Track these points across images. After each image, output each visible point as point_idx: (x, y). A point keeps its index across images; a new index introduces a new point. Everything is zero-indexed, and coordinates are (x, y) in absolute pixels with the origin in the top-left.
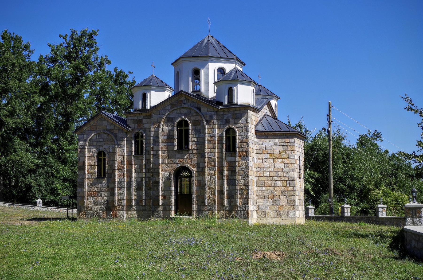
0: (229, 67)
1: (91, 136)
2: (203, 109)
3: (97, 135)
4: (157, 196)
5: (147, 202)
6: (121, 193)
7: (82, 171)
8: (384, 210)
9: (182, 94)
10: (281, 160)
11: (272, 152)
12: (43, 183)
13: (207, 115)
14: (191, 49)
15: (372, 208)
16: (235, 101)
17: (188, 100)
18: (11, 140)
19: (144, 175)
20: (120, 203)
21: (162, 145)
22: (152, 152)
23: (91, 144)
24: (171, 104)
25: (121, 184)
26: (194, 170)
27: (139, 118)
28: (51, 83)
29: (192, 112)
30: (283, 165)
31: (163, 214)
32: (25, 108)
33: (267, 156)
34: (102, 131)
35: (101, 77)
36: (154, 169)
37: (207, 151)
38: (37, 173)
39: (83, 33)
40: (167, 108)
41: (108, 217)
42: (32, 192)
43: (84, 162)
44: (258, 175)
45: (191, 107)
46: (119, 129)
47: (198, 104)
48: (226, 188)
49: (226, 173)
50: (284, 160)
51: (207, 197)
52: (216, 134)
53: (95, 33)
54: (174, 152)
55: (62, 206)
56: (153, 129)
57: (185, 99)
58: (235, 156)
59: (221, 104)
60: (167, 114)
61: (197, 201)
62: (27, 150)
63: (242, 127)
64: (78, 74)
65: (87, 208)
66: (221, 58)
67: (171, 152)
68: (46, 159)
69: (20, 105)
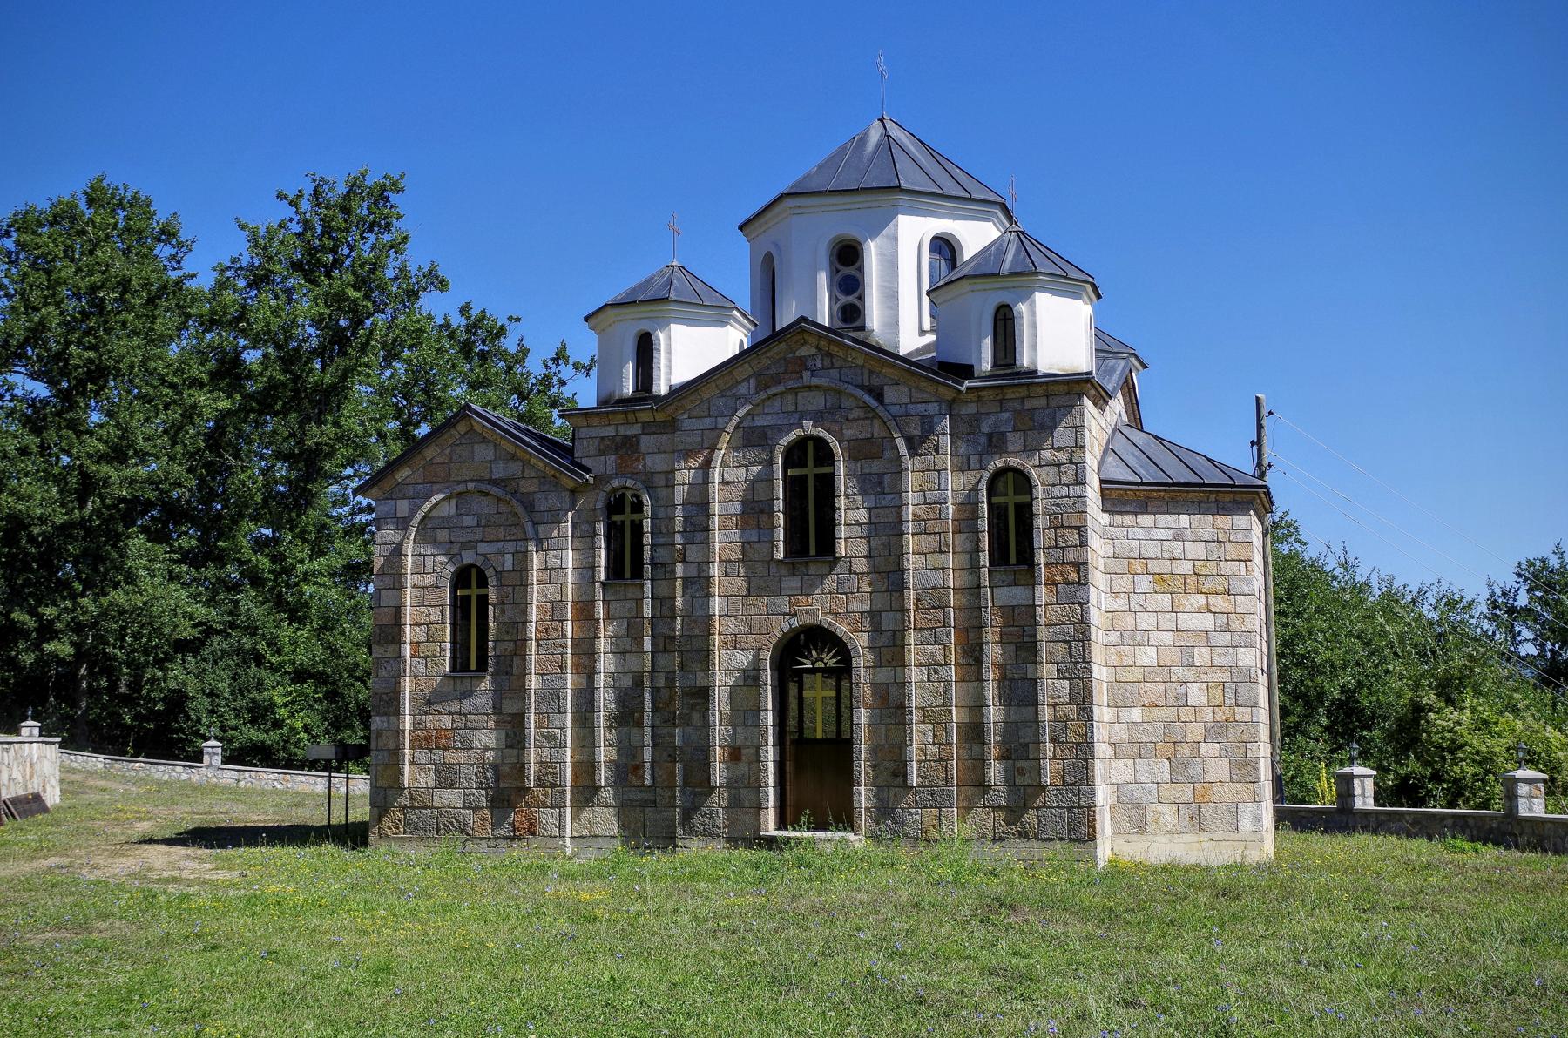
0: (976, 236)
1: (427, 506)
2: (890, 394)
3: (453, 502)
4: (705, 750)
5: (659, 772)
6: (550, 737)
7: (391, 648)
8: (1535, 792)
9: (804, 330)
10: (1202, 599)
11: (1163, 567)
12: (224, 687)
13: (908, 415)
14: (820, 167)
15: (1437, 778)
16: (1025, 360)
17: (830, 355)
18: (116, 538)
19: (648, 666)
20: (549, 780)
21: (723, 539)
22: (680, 570)
23: (427, 535)
24: (757, 375)
25: (551, 697)
26: (860, 642)
27: (623, 431)
28: (252, 357)
29: (846, 404)
30: (1207, 622)
31: (731, 823)
32: (165, 432)
33: (1144, 583)
34: (471, 486)
35: (421, 330)
36: (688, 637)
37: (912, 562)
38: (206, 653)
39: (354, 188)
40: (743, 389)
41: (499, 832)
42: (188, 718)
43: (398, 610)
44: (1114, 661)
45: (842, 386)
46: (543, 478)
47: (871, 372)
48: (994, 713)
49: (993, 651)
50: (1213, 599)
51: (914, 753)
52: (949, 493)
53: (394, 183)
54: (773, 570)
55: (292, 763)
56: (685, 475)
57: (813, 351)
58: (1032, 583)
59: (966, 371)
60: (741, 413)
61: (874, 767)
62: (170, 573)
63: (1059, 466)
64: (342, 323)
65: (411, 798)
66: (943, 196)
67: (760, 569)
68: (236, 603)
69: (147, 420)
